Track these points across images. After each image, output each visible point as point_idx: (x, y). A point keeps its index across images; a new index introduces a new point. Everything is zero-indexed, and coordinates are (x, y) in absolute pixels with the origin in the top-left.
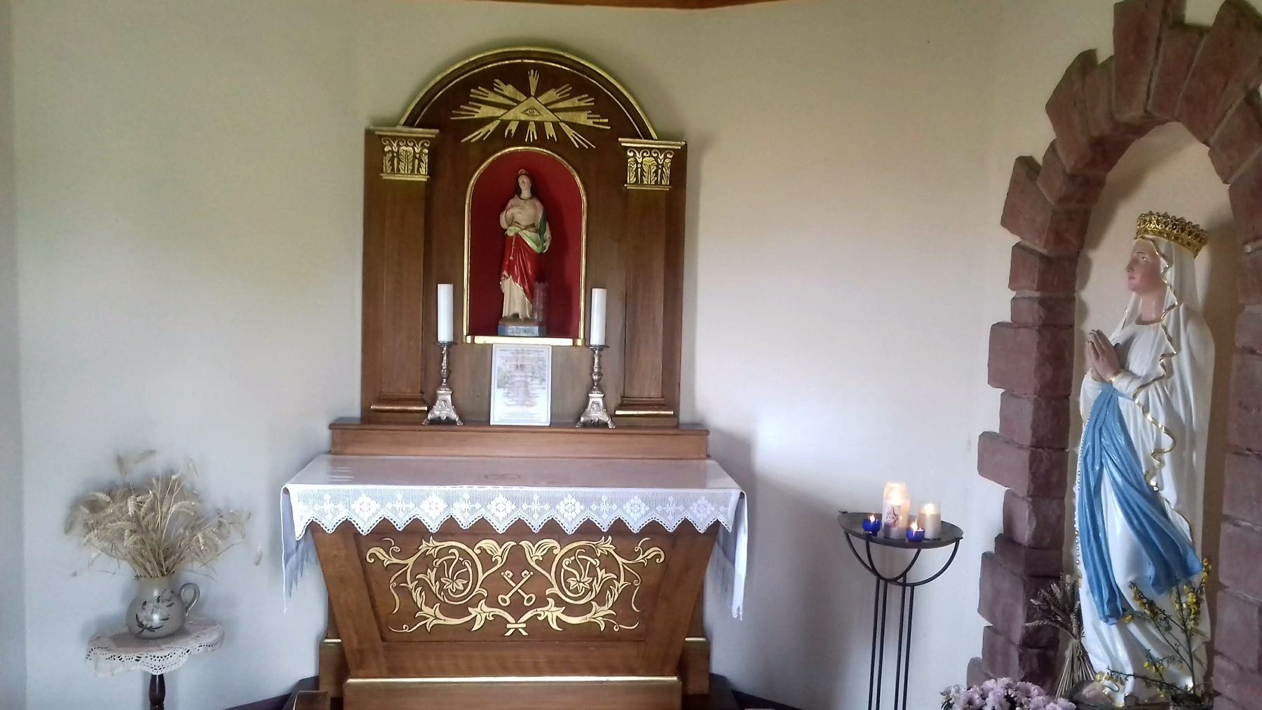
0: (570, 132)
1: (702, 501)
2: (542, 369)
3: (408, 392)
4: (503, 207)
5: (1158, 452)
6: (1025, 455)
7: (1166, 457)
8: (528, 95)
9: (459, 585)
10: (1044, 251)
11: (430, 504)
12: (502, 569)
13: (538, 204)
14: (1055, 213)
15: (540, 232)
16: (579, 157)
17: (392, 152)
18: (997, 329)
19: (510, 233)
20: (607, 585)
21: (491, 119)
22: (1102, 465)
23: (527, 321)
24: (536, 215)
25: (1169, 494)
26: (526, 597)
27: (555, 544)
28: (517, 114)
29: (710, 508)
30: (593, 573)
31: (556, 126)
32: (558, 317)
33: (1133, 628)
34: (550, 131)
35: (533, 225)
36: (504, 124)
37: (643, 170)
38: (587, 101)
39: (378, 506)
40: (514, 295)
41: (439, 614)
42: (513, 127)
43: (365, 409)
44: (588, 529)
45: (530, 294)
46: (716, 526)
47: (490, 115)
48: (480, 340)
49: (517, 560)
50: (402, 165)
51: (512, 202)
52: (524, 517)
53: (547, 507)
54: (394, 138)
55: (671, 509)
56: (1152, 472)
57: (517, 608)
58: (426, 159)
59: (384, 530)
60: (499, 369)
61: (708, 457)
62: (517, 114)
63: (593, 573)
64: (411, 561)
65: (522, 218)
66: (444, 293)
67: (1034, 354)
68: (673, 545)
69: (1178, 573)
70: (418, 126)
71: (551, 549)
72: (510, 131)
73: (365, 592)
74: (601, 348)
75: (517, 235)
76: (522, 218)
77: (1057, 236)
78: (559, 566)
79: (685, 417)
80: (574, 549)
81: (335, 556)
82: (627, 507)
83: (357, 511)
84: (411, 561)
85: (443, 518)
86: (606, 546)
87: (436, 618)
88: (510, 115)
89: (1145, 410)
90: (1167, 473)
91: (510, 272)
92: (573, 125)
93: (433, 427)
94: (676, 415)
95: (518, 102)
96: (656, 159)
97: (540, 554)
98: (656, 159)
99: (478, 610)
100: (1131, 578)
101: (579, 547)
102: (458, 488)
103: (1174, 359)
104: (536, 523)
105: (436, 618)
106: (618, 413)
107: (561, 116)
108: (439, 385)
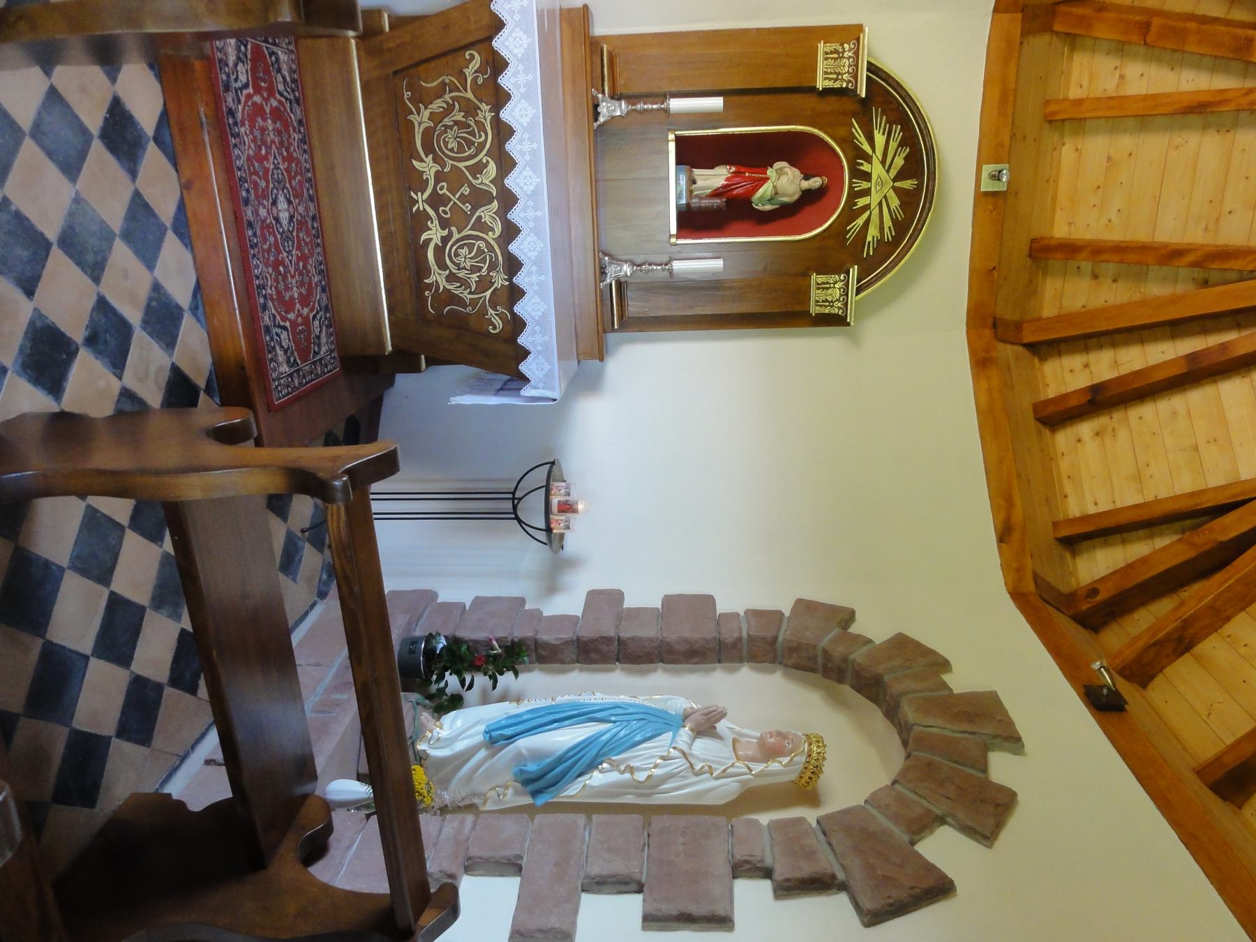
0: (860, 221)
1: (547, 367)
3: (620, 82)
4: (792, 164)
5: (631, 770)
6: (611, 633)
7: (627, 776)
8: (894, 180)
9: (453, 144)
10: (780, 639)
11: (524, 111)
12: (471, 185)
13: (796, 197)
14: (815, 646)
15: (770, 200)
16: (838, 231)
17: (843, 52)
18: (709, 601)
19: (770, 172)
20: (464, 283)
22: (614, 722)
23: (690, 192)
24: (784, 195)
25: (597, 779)
27: (498, 232)
29: (540, 375)
30: (474, 269)
31: (867, 207)
33: (482, 753)
34: (862, 202)
35: (776, 193)
36: (868, 159)
38: (888, 235)
40: (715, 177)
41: (423, 126)
42: (866, 167)
44: (513, 265)
45: (716, 194)
46: (525, 380)
48: (672, 147)
49: (479, 198)
54: (857, 53)
55: (538, 338)
56: (615, 766)
57: (436, 201)
58: (837, 85)
59: (497, 64)
62: (876, 169)
63: (474, 269)
64: (470, 95)
65: (784, 181)
67: (696, 636)
68: (506, 341)
69: (532, 787)
70: (868, 77)
71: (492, 230)
76: (784, 181)
77: (794, 649)
78: (478, 238)
79: (611, 337)
80: (494, 251)
84: (470, 95)
85: (514, 124)
86: (500, 280)
88: (876, 162)
89: (663, 758)
90: (614, 776)
93: (591, 107)
94: (613, 330)
95: (888, 171)
96: (838, 300)
97: (486, 219)
98: (838, 300)
99: (431, 164)
100: (524, 752)
101: (496, 256)
103: (707, 775)
104: (515, 215)
107: (876, 212)
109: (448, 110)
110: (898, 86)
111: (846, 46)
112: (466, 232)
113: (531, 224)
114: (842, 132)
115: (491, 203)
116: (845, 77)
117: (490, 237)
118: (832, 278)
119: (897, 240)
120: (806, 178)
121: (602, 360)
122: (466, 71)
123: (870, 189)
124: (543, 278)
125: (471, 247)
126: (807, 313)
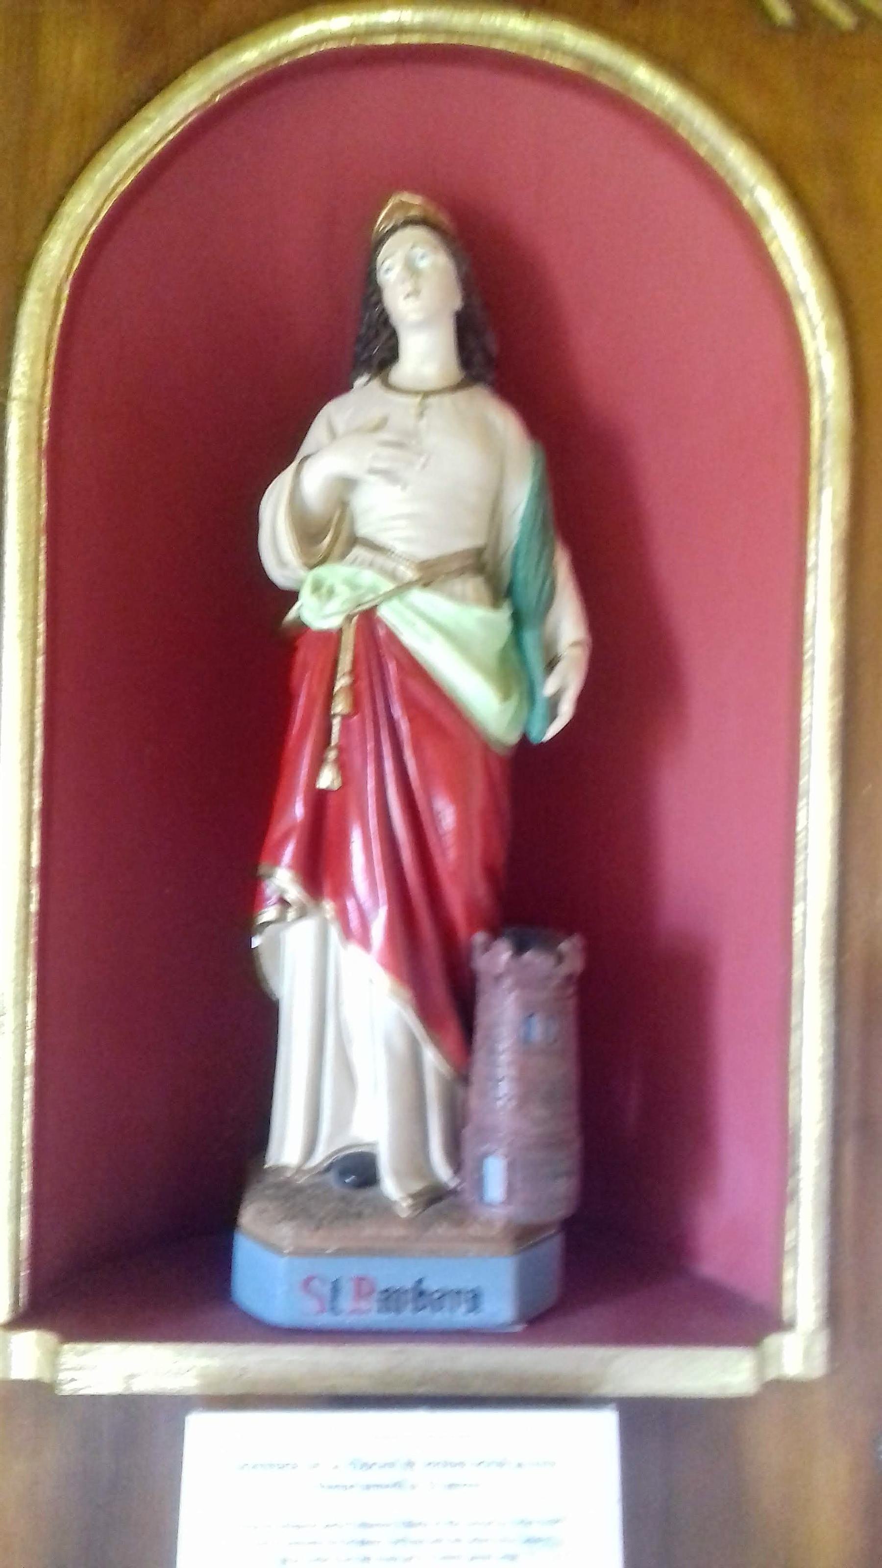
4: (282, 445)
13: (506, 423)
40: (343, 1023)
45: (447, 998)
51: (336, 414)
91: (321, 870)
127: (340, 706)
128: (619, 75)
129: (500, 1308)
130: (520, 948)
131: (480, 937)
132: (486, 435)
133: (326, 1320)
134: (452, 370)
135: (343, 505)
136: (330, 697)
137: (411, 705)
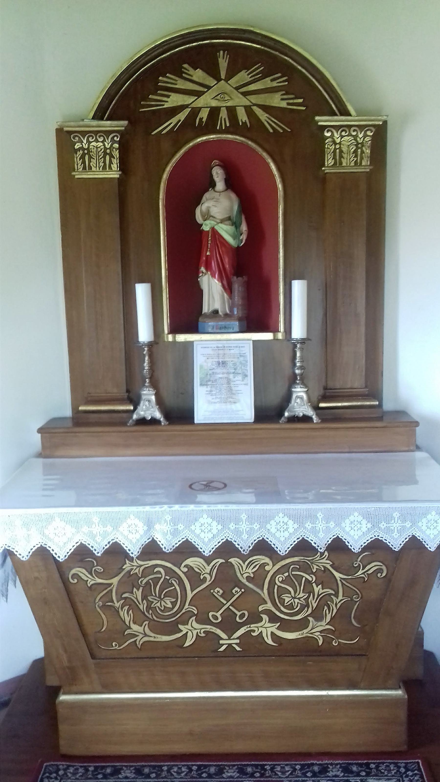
0: (263, 116)
2: (244, 364)
4: (198, 202)
8: (219, 80)
13: (233, 196)
15: (236, 225)
16: (274, 142)
17: (83, 149)
19: (206, 228)
20: (324, 602)
21: (182, 108)
26: (239, 614)
27: (267, 560)
28: (207, 101)
30: (310, 591)
31: (248, 110)
32: (257, 313)
34: (242, 116)
35: (229, 218)
36: (195, 112)
37: (341, 152)
39: (74, 530)
40: (213, 291)
42: (204, 115)
43: (75, 410)
45: (228, 288)
47: (180, 104)
48: (181, 338)
50: (93, 162)
51: (207, 195)
52: (232, 537)
53: (256, 526)
54: (84, 134)
57: (229, 625)
58: (116, 154)
59: (82, 554)
60: (201, 367)
61: (418, 448)
62: (207, 101)
64: (115, 581)
65: (217, 210)
66: (142, 292)
71: (263, 565)
72: (201, 119)
73: (70, 612)
74: (303, 341)
75: (213, 229)
78: (272, 583)
79: (388, 405)
81: (36, 578)
82: (346, 524)
83: (52, 536)
84: (115, 581)
85: (145, 540)
87: (146, 635)
88: (201, 102)
91: (208, 267)
92: (266, 108)
94: (380, 406)
97: (250, 571)
98: (355, 137)
99: (189, 627)
101: (293, 563)
102: (157, 508)
104: (245, 543)
105: (146, 635)
106: (322, 405)
107: (254, 99)
108: (143, 385)
109: (132, 605)
110: (118, 83)
111: (76, 147)
112: (265, 594)
113: (256, 526)
114: (166, 145)
115: (232, 565)
116: (108, 146)
117: (271, 568)
118: (329, 147)
119: (287, 70)
120: (213, 185)
121: (417, 424)
122: (90, 583)
123: (228, 108)
124: (320, 515)
125: (283, 591)
126: (369, 176)
127: (209, 242)
128: (247, 143)
129: (237, 329)
130: (237, 277)
131: (232, 276)
132: (230, 199)
133: (212, 331)
134: (235, 110)
135: (209, 211)
136: (208, 241)
137: (220, 242)
